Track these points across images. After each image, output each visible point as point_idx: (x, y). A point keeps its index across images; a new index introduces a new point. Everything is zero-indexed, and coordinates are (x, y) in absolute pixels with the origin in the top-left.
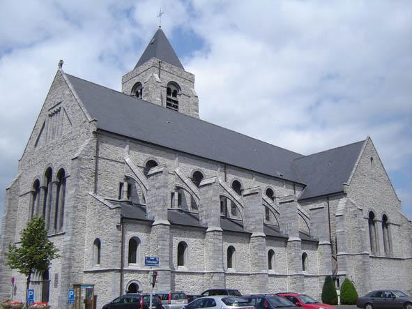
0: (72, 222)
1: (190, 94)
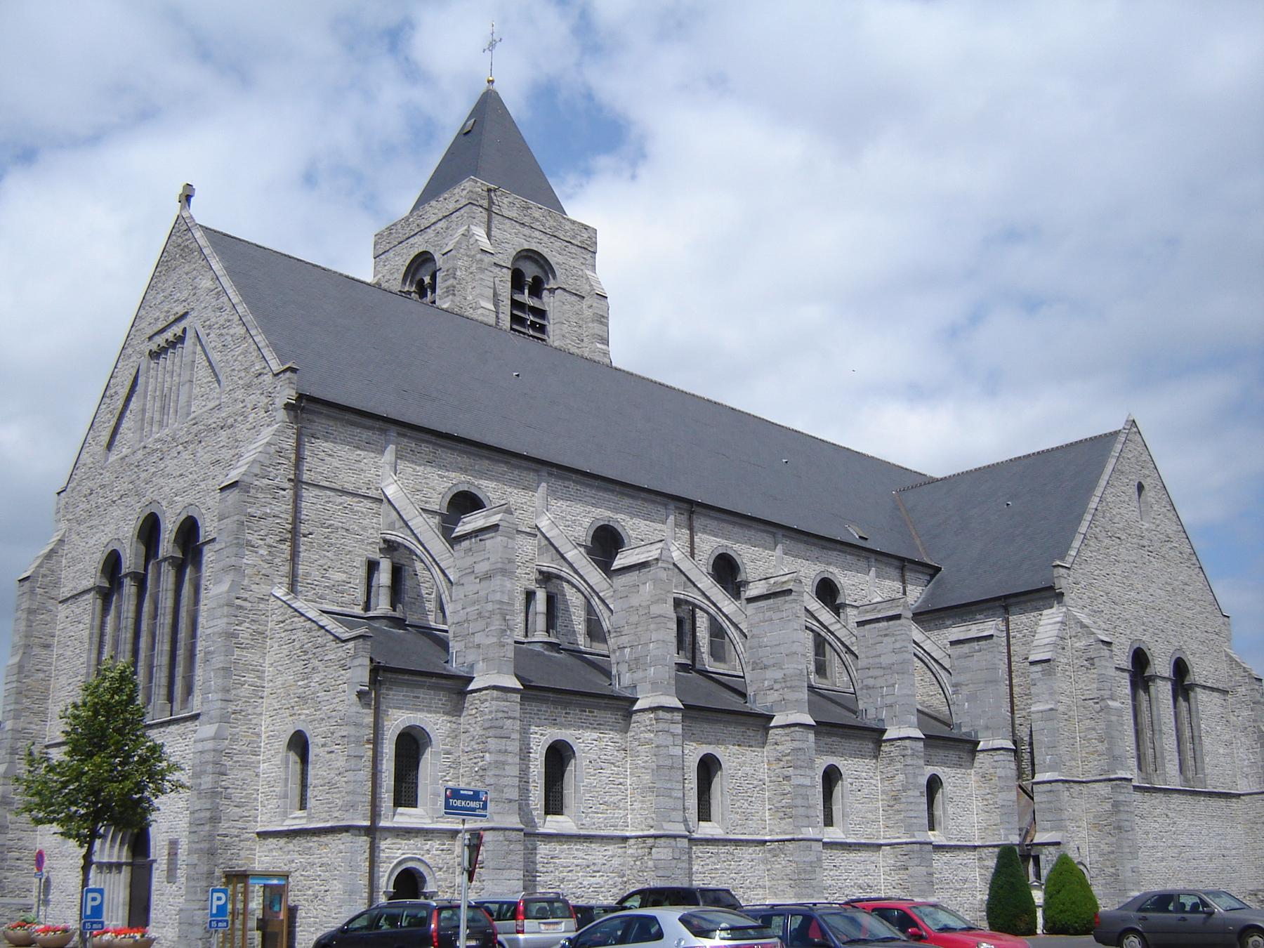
1: (585, 289)
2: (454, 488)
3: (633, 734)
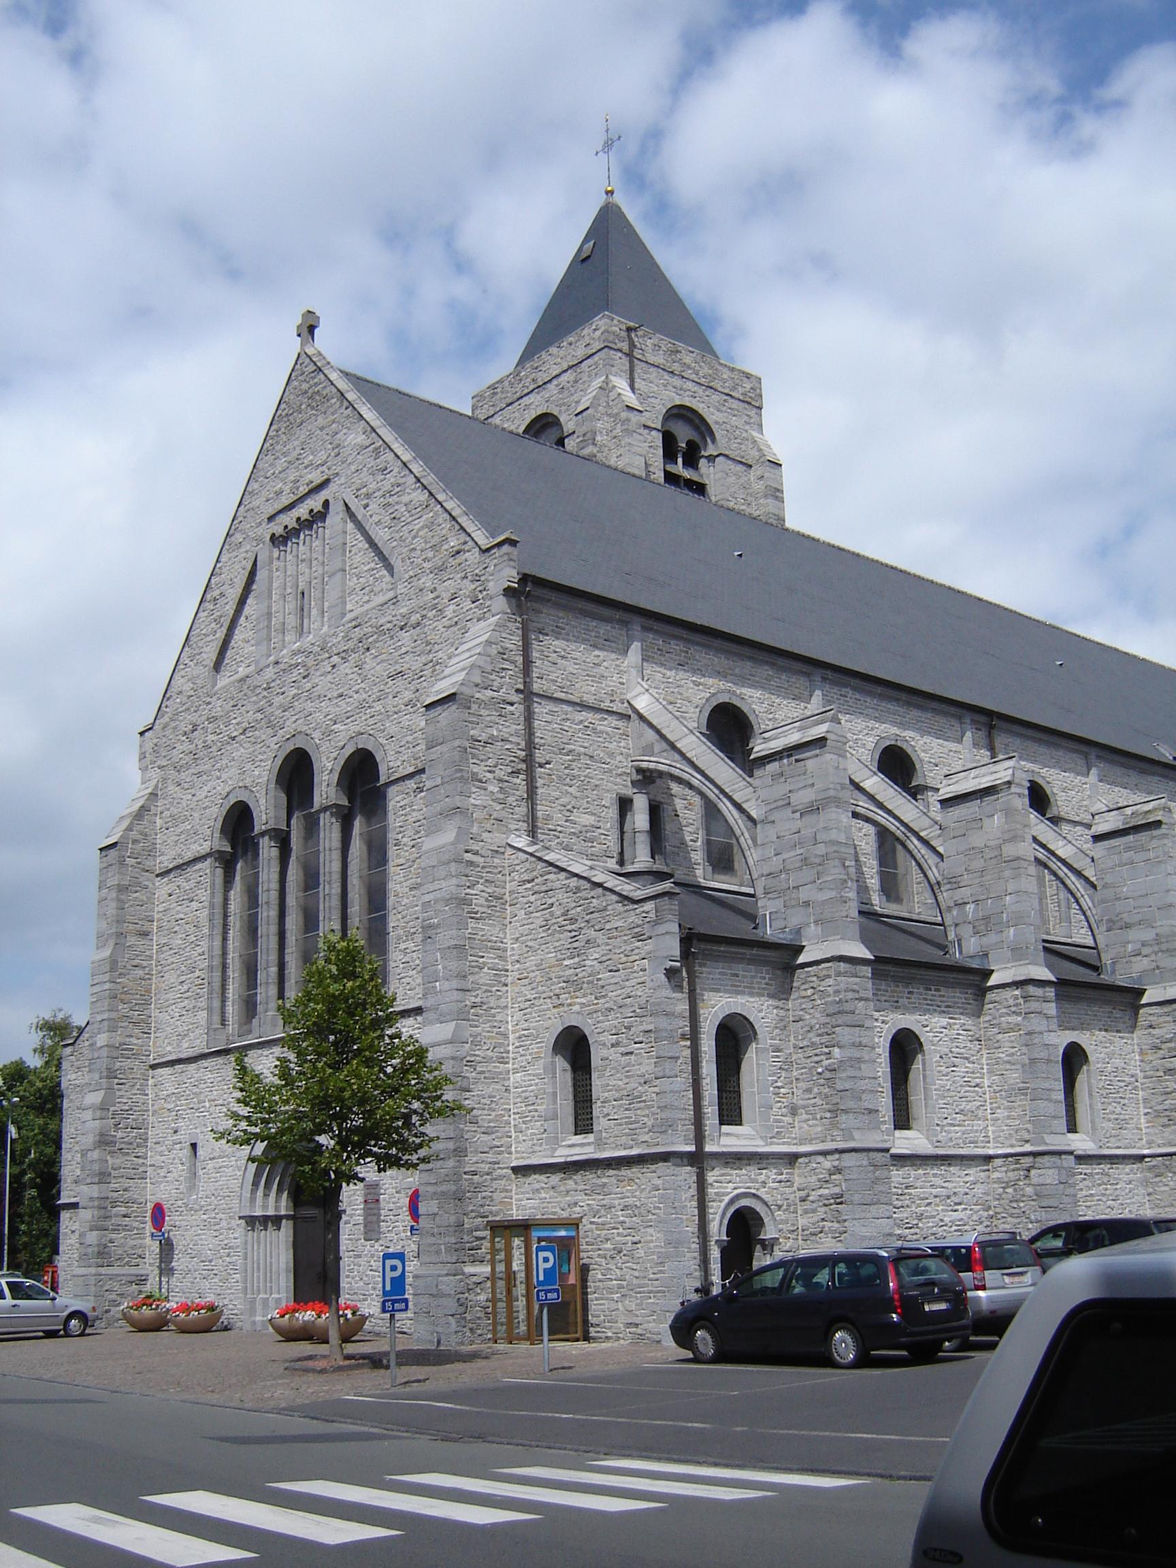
0: (453, 965)
1: (751, 455)
2: (713, 699)
3: (987, 1018)
